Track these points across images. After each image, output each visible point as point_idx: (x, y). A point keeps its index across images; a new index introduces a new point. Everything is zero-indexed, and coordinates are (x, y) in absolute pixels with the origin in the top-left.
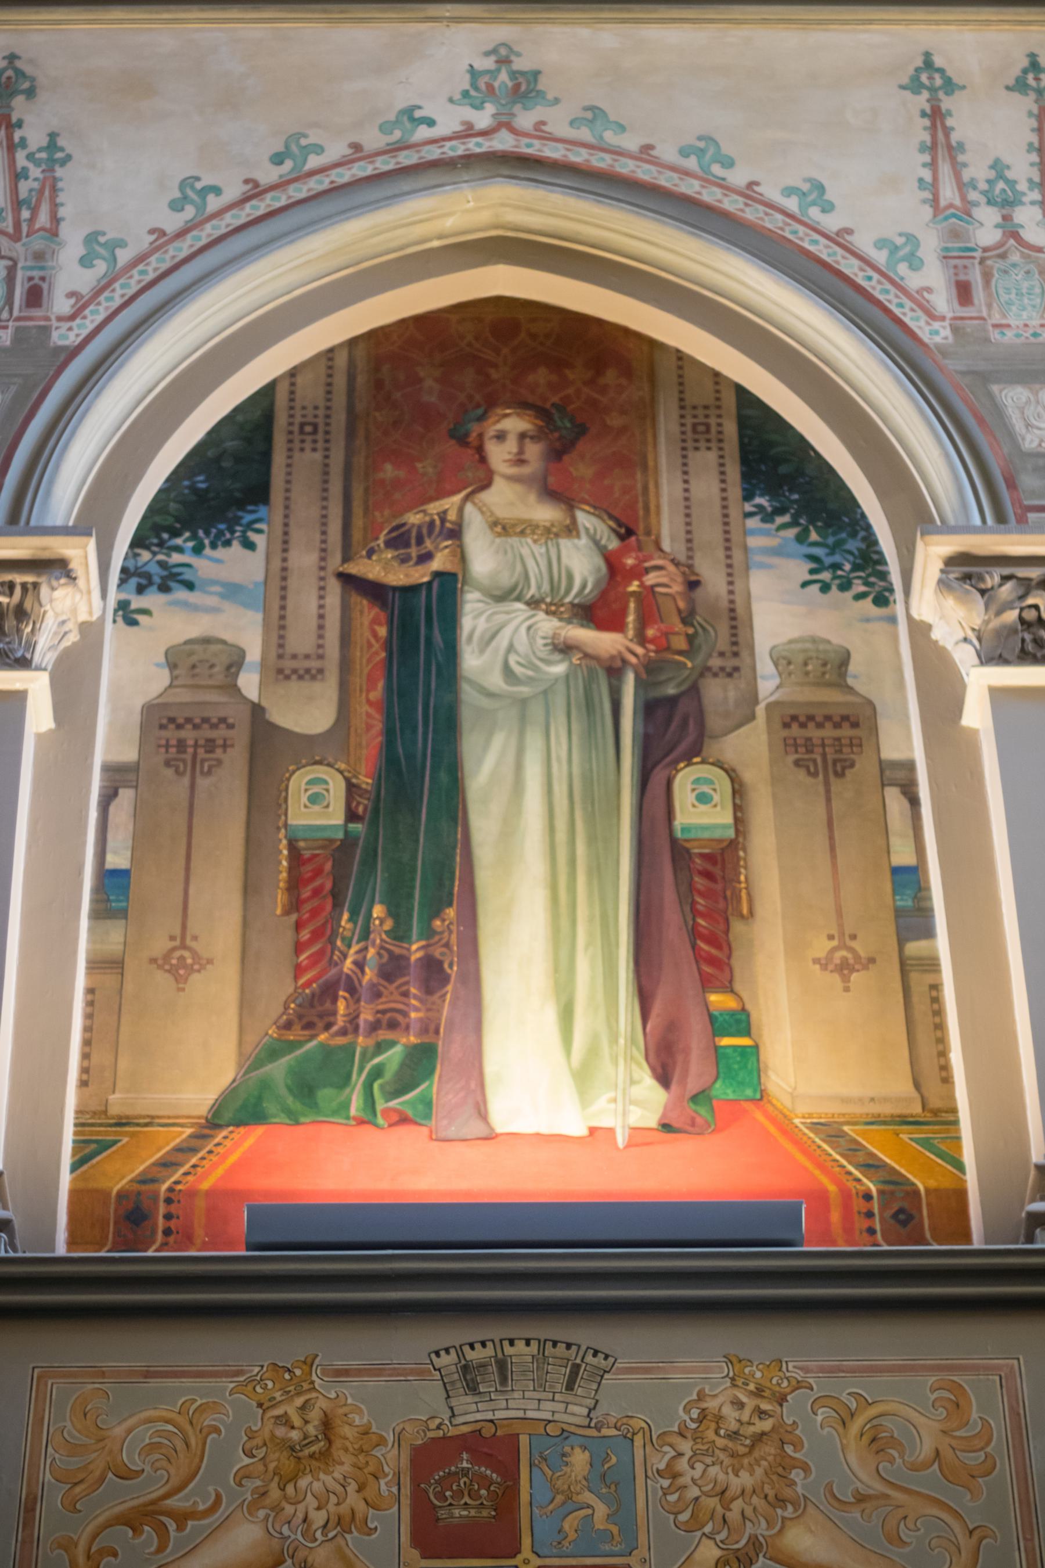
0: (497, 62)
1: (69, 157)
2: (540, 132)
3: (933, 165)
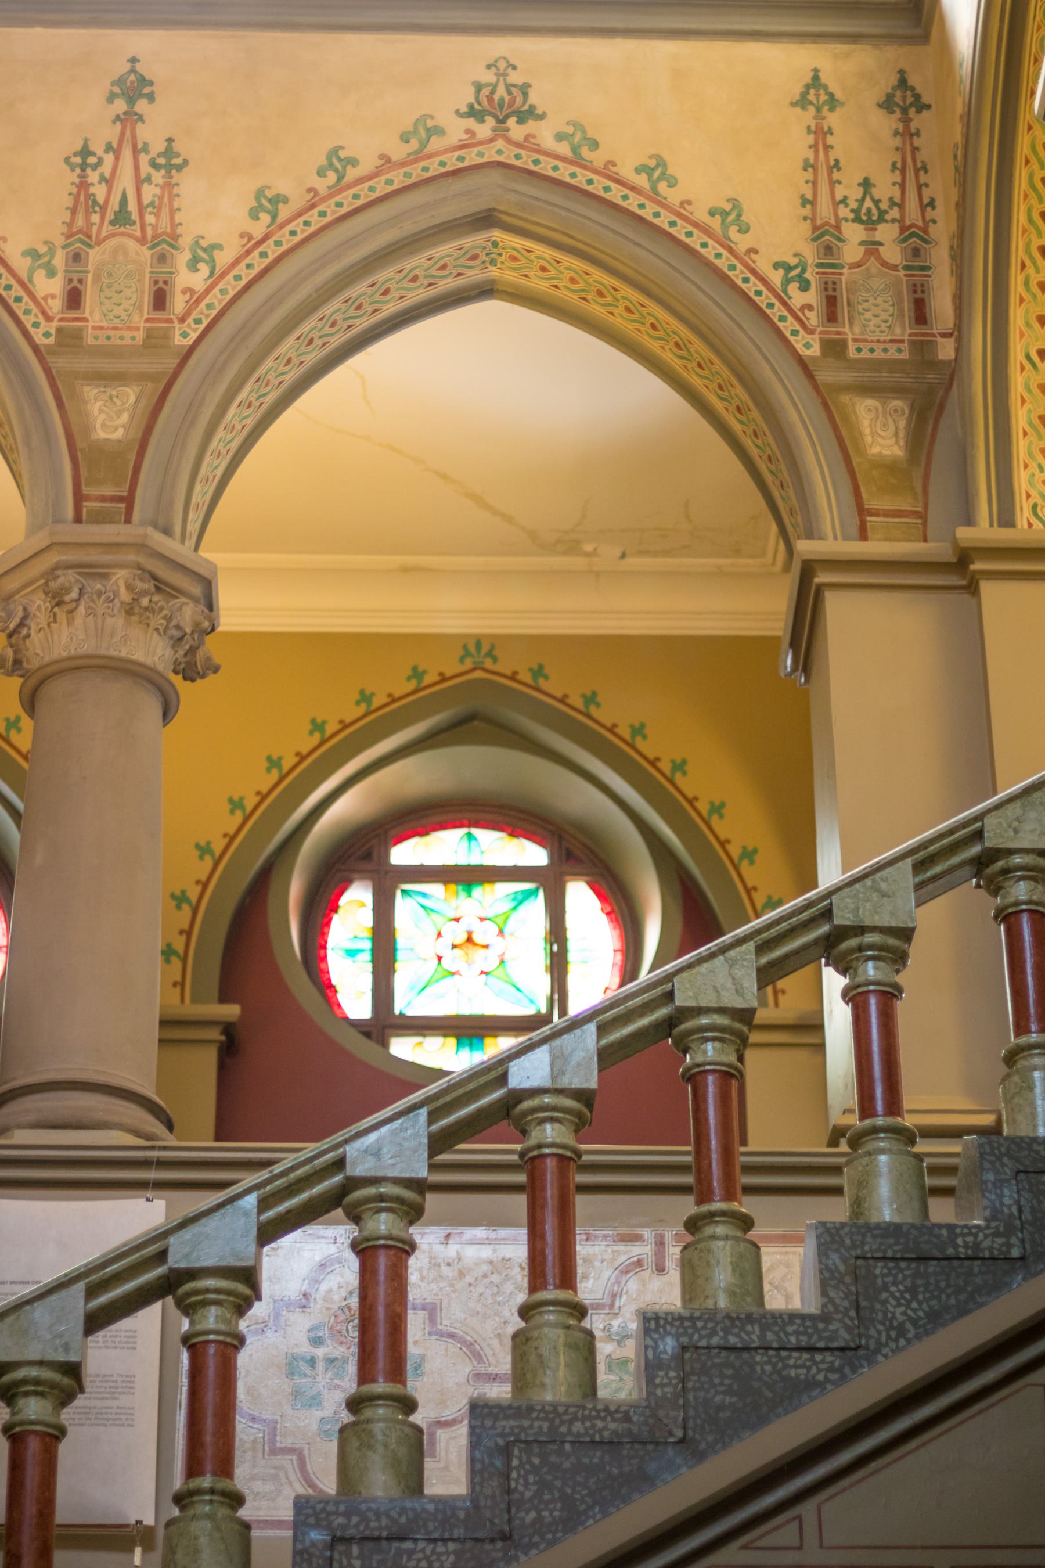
0: (507, 75)
1: (186, 162)
2: (528, 144)
3: (902, 186)
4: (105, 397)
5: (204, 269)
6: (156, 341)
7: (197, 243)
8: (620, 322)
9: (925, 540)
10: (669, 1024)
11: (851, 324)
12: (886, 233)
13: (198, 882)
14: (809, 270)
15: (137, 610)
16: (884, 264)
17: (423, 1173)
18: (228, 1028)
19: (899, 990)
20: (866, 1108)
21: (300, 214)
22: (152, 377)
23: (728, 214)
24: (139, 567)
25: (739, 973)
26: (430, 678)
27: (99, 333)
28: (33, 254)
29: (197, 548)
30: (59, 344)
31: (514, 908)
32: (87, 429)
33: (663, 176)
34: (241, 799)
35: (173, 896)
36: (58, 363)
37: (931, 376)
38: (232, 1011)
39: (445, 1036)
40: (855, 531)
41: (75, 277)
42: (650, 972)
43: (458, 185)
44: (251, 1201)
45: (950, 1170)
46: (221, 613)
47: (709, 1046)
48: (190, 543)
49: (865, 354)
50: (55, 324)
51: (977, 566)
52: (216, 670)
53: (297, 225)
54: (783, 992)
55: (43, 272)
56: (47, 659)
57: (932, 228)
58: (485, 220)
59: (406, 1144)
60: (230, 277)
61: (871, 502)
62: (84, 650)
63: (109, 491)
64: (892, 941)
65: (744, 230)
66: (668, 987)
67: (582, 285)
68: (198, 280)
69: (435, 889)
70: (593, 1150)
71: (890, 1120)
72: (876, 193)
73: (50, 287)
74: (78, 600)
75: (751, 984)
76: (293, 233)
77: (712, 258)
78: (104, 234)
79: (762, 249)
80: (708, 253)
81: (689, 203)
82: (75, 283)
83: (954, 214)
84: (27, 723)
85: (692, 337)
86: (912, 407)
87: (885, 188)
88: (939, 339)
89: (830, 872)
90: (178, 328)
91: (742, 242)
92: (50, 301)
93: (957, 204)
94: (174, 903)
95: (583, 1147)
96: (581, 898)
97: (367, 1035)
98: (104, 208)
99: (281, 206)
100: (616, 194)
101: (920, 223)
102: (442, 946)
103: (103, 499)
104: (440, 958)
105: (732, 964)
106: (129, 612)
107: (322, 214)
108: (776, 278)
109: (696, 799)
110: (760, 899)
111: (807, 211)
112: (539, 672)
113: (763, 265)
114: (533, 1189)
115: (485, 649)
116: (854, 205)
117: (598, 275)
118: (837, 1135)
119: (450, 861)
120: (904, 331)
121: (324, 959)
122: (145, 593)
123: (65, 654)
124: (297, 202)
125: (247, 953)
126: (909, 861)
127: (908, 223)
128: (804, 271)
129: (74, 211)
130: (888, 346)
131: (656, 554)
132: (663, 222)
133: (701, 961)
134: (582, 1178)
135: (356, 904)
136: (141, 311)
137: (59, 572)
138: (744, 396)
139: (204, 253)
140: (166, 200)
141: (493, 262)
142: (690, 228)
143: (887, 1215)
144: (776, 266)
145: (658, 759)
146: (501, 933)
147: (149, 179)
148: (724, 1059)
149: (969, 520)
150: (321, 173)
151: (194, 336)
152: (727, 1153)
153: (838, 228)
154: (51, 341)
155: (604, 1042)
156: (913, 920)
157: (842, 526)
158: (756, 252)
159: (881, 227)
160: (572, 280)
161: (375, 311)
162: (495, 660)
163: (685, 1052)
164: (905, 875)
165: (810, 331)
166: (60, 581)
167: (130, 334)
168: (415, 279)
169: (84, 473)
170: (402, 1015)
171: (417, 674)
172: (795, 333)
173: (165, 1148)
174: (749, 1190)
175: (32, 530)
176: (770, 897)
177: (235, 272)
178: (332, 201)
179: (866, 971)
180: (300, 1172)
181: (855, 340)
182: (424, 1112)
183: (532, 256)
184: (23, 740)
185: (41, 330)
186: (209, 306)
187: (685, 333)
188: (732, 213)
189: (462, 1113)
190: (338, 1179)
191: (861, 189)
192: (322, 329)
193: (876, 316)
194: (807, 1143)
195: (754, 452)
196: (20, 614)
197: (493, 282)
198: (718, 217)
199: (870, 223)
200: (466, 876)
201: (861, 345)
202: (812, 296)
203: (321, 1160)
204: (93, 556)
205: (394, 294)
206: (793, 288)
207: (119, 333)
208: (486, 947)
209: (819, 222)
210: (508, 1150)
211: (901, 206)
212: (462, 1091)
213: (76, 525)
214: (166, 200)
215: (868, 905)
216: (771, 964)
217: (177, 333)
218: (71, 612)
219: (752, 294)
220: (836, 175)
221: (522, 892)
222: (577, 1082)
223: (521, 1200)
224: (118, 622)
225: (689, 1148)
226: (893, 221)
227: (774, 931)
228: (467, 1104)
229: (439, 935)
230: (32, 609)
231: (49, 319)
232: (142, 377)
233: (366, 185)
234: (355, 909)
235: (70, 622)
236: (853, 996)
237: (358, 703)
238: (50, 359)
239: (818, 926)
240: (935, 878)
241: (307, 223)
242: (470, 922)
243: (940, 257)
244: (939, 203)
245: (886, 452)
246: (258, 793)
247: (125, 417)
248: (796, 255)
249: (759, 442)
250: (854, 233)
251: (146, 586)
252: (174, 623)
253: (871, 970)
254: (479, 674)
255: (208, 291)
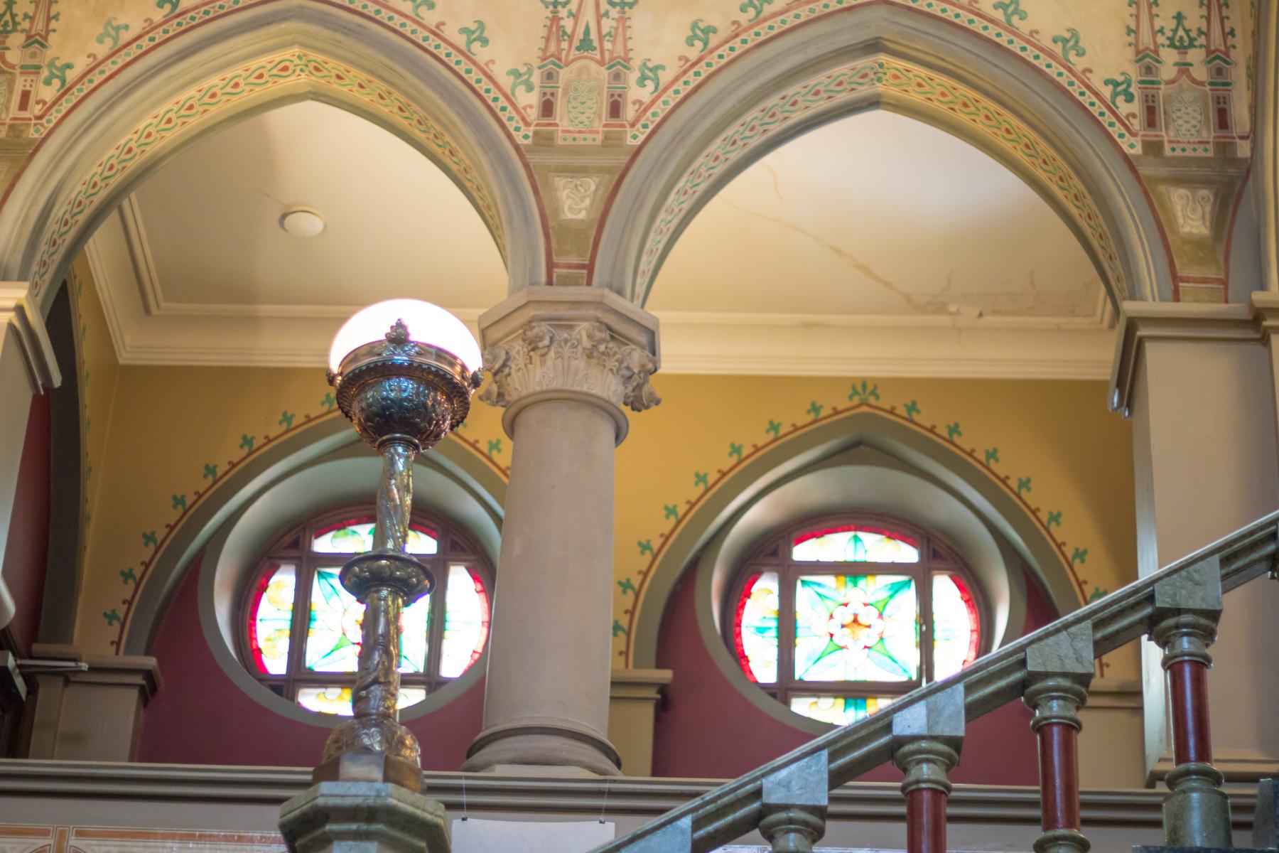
3: (1208, 18)
4: (572, 186)
5: (650, 85)
6: (611, 142)
7: (645, 64)
8: (981, 127)
9: (1226, 301)
10: (1022, 686)
11: (1167, 129)
12: (1196, 56)
13: (640, 572)
14: (1133, 85)
15: (595, 354)
16: (1194, 81)
17: (825, 802)
18: (663, 689)
19: (1209, 660)
20: (1181, 756)
21: (726, 42)
22: (609, 171)
23: (1068, 41)
24: (598, 320)
25: (1079, 645)
26: (826, 411)
27: (567, 135)
28: (515, 73)
29: (643, 306)
30: (536, 144)
31: (891, 596)
32: (557, 211)
33: (1016, 11)
34: (675, 507)
35: (620, 583)
36: (534, 159)
37: (1231, 171)
38: (666, 675)
39: (836, 697)
40: (1169, 294)
41: (549, 91)
42: (1001, 646)
43: (852, 19)
44: (686, 822)
45: (1249, 809)
46: (663, 359)
47: (1055, 704)
48: (638, 302)
49: (1178, 153)
50: (532, 128)
51: (1266, 323)
52: (658, 402)
53: (724, 50)
54: (1108, 665)
55: (523, 87)
56: (524, 393)
57: (1232, 53)
58: (874, 46)
59: (811, 779)
60: (671, 91)
61: (1183, 272)
62: (555, 385)
63: (574, 260)
64: (1203, 621)
65: (1081, 54)
66: (1021, 656)
67: (950, 98)
68: (646, 94)
69: (829, 580)
70: (961, 788)
71: (1201, 765)
72: (1187, 24)
73: (529, 100)
74: (549, 346)
75: (1088, 652)
76: (721, 57)
77: (1055, 76)
78: (571, 57)
79: (1095, 68)
80: (1052, 72)
81: (1037, 32)
82: (548, 96)
83: (1250, 41)
84: (507, 444)
85: (1039, 139)
86: (1216, 196)
87: (1194, 20)
88: (1238, 141)
89: (1149, 567)
90: (629, 132)
91: (1079, 64)
92: (529, 110)
93: (1253, 33)
94: (621, 588)
95: (954, 785)
96: (944, 588)
97: (774, 695)
98: (571, 37)
99: (711, 35)
100: (978, 25)
101: (1223, 48)
102: (834, 627)
103: (570, 266)
104: (832, 635)
105: (1073, 637)
106: (590, 356)
107: (744, 42)
108: (1107, 92)
109: (1038, 510)
110: (1089, 590)
111: (1132, 39)
112: (912, 407)
113: (1097, 82)
114: (912, 819)
115: (870, 388)
116: (1169, 34)
117: (964, 90)
118: (1154, 778)
119: (840, 557)
120: (1210, 134)
121: (739, 635)
122: (601, 341)
123: (538, 389)
124: (724, 31)
125: (679, 631)
126: (1217, 557)
127: (1213, 48)
128: (1129, 86)
129: (548, 40)
130: (1196, 146)
131: (1007, 314)
132: (1016, 47)
133: (1048, 635)
134: (951, 811)
135: (765, 591)
136: (600, 119)
137: (535, 324)
138: (1081, 187)
139: (650, 72)
140: (620, 31)
141: (879, 80)
142: (1037, 52)
143: (1198, 841)
144: (1107, 82)
145: (1008, 478)
146: (880, 616)
147: (607, 14)
148: (1067, 714)
149: (1262, 286)
150: (743, 9)
151: (642, 138)
152: (1069, 787)
153: (1156, 52)
154: (529, 141)
155: (970, 699)
156: (1220, 604)
157: (1159, 290)
158: (1090, 71)
159: (1191, 52)
160: (943, 94)
161: (786, 118)
162: (877, 397)
163: (1035, 707)
164: (1213, 567)
165: (1134, 135)
166: (535, 331)
167: (590, 136)
168: (817, 93)
169: (554, 246)
170: (801, 680)
171: (815, 408)
172: (1121, 136)
173: (615, 781)
174: (1087, 822)
175: (513, 291)
176: (1097, 589)
177: (675, 87)
178: (752, 32)
179: (1181, 645)
180: (726, 799)
181: (1170, 142)
182: (825, 753)
183: (910, 75)
184: (504, 458)
185: (521, 133)
186: (654, 114)
187: (1033, 135)
188: (1071, 41)
189: (856, 754)
190: (756, 805)
191: (1175, 22)
192: (744, 133)
193: (1187, 122)
194: (1126, 784)
195: (1088, 231)
196: (503, 357)
197: (879, 95)
198: (1060, 44)
199: (1182, 48)
200: (853, 570)
201: (1175, 146)
202: (1136, 107)
203: (743, 790)
204: (562, 312)
205: (801, 105)
206: (1120, 100)
207: (583, 136)
208: (869, 626)
209: (1141, 48)
210: (892, 787)
211: (1207, 35)
212: (855, 737)
213: (548, 288)
214: (620, 31)
215: (1184, 592)
216: (1105, 638)
217: (629, 135)
218: (543, 355)
219: (1087, 105)
220: (1155, 10)
221: (893, 585)
222: (948, 731)
223: (901, 829)
224: (580, 363)
225: (1038, 788)
226: (1201, 46)
227: (1107, 612)
228: (859, 747)
229: (831, 617)
230: (513, 353)
231: (527, 124)
232: (600, 170)
233: (779, 19)
234: (764, 596)
235: (543, 363)
236: (1171, 665)
237: (768, 431)
238: (528, 156)
239: (1144, 608)
240: (1238, 570)
241: (732, 49)
242: (856, 607)
243: (1239, 75)
244: (1238, 32)
245: (1195, 231)
246: (688, 502)
247: (587, 202)
248: (1122, 74)
249: (1092, 223)
250: (1169, 57)
251: (603, 335)
252: (625, 364)
253: (1185, 644)
254: (864, 409)
255: (653, 102)
